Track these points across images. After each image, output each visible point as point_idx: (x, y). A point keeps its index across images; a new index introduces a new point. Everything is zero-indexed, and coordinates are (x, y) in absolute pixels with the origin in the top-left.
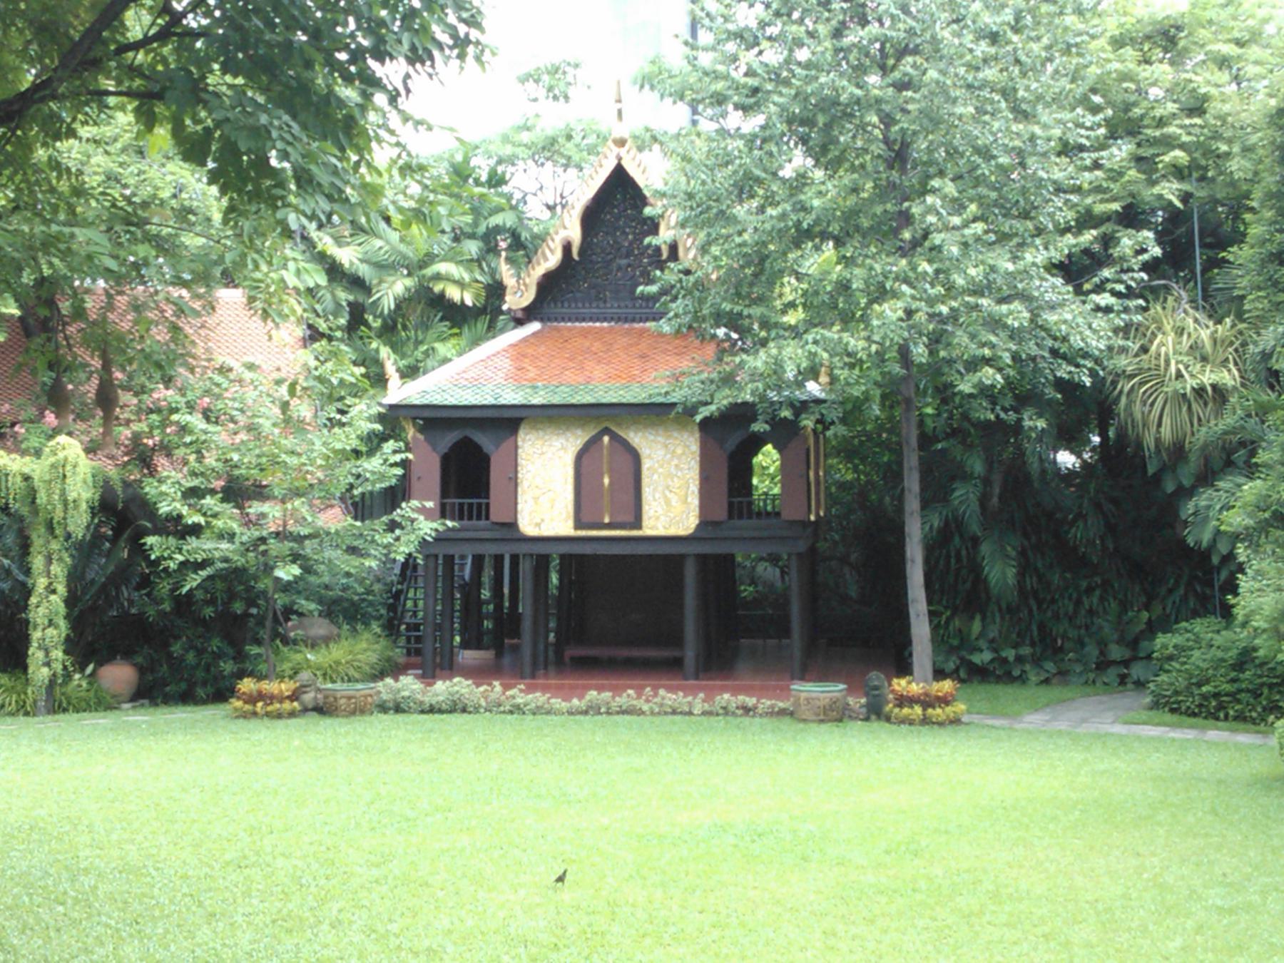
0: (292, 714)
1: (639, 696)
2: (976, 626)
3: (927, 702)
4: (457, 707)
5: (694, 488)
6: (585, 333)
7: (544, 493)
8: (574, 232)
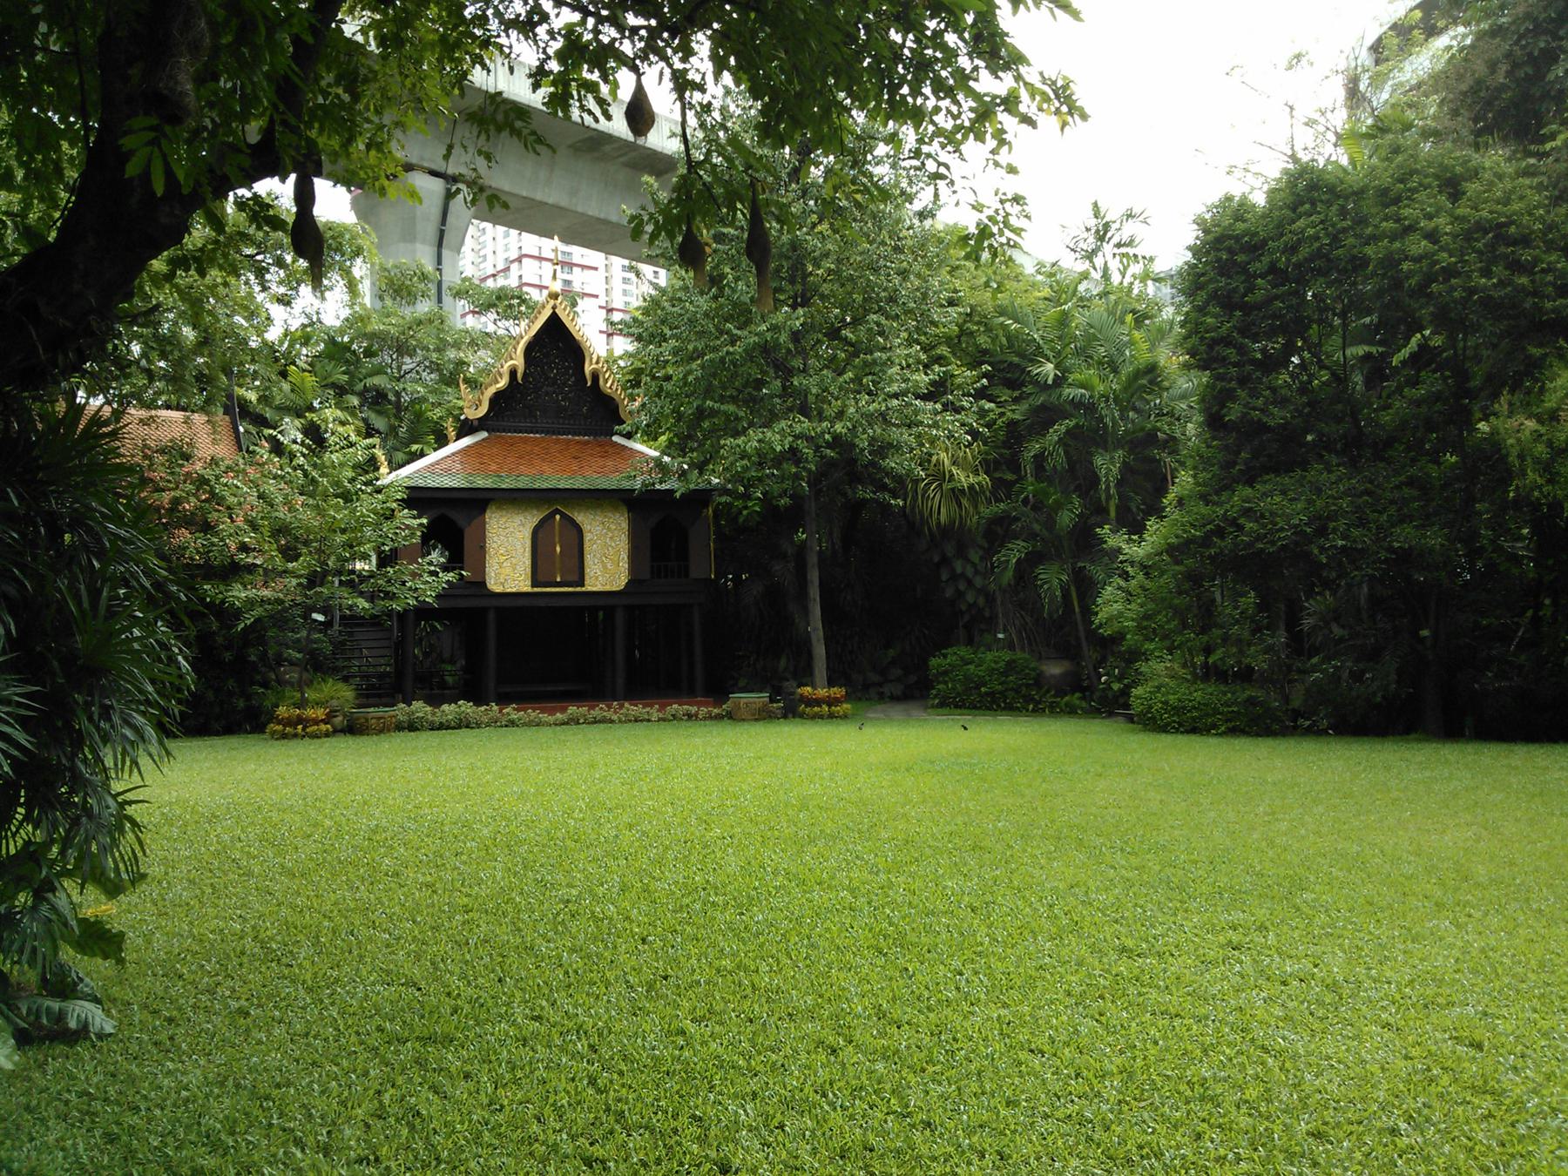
0: (327, 735)
1: (609, 707)
2: (783, 663)
3: (832, 702)
4: (462, 724)
5: (624, 556)
6: (525, 441)
7: (508, 558)
8: (519, 361)
